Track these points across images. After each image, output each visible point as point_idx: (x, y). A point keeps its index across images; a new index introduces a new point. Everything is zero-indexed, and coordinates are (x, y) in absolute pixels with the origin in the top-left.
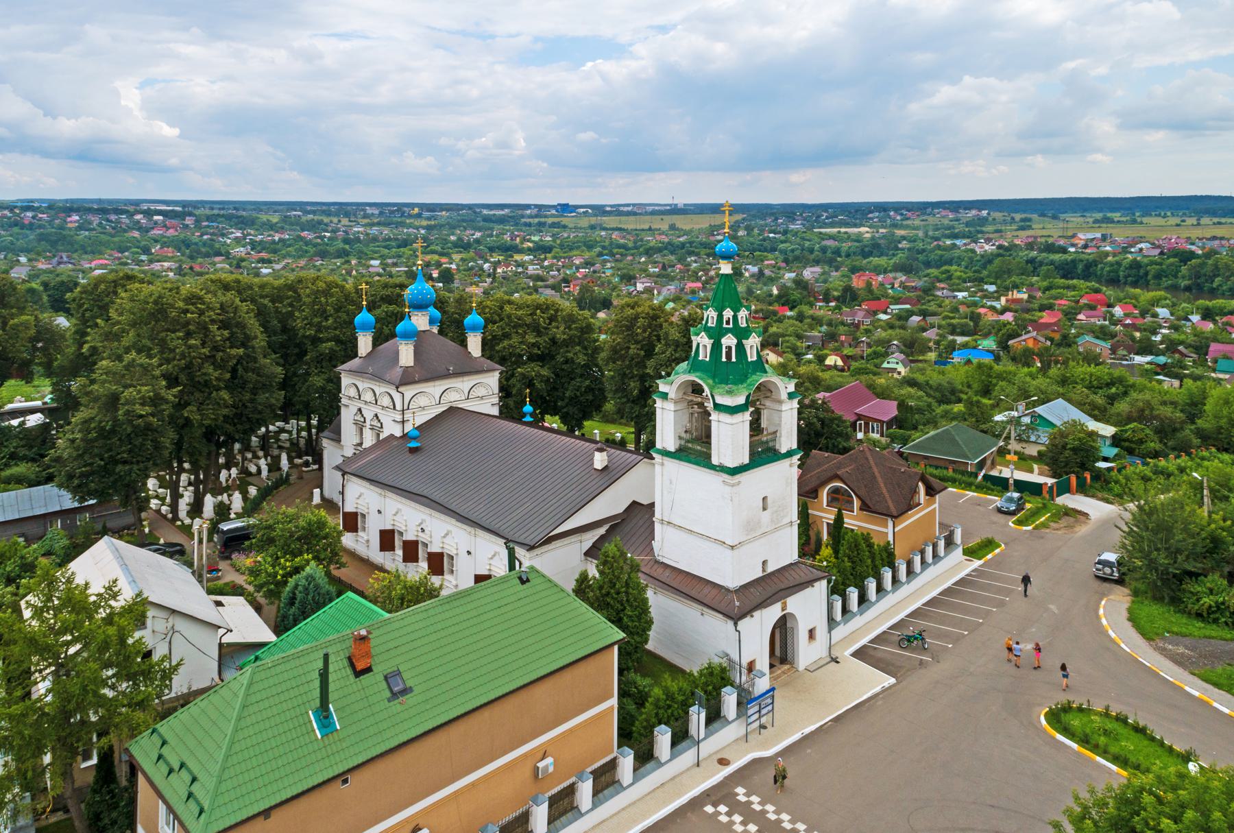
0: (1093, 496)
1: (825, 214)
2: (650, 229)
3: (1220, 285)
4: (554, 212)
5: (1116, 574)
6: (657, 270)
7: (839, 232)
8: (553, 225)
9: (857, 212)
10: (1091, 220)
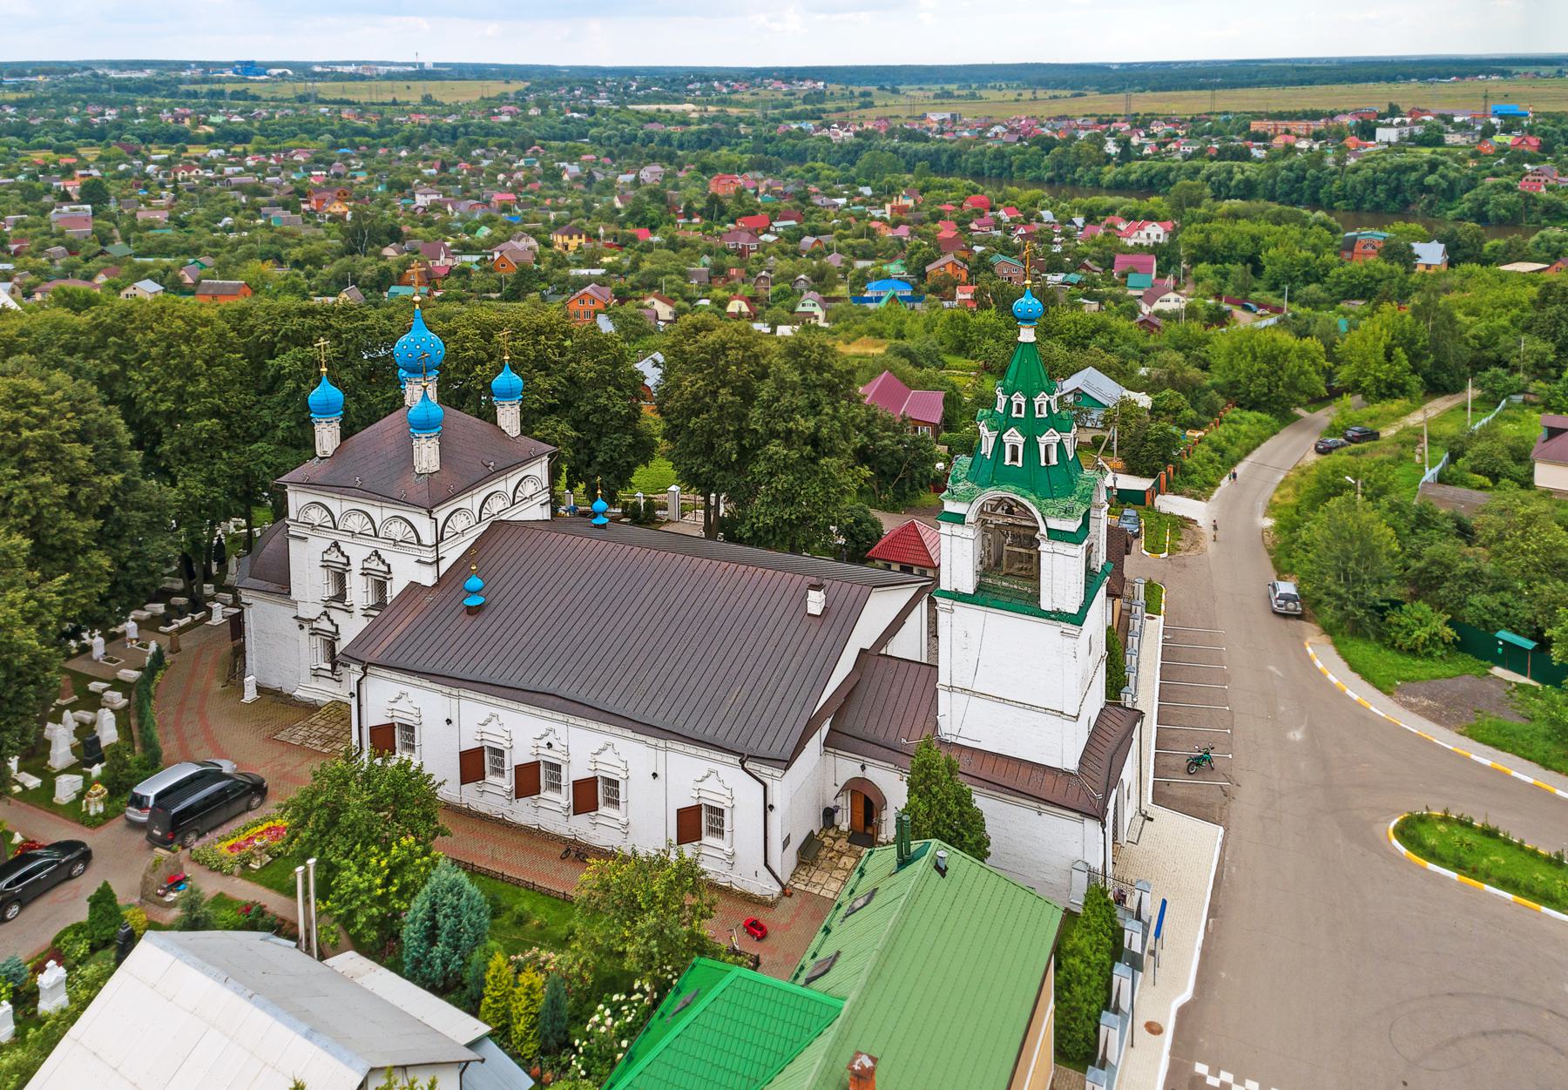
0: (1181, 494)
1: (635, 84)
2: (394, 103)
3: (1082, 176)
4: (230, 73)
5: (1299, 609)
6: (434, 171)
7: (659, 110)
8: (236, 95)
9: (674, 82)
10: (931, 94)
